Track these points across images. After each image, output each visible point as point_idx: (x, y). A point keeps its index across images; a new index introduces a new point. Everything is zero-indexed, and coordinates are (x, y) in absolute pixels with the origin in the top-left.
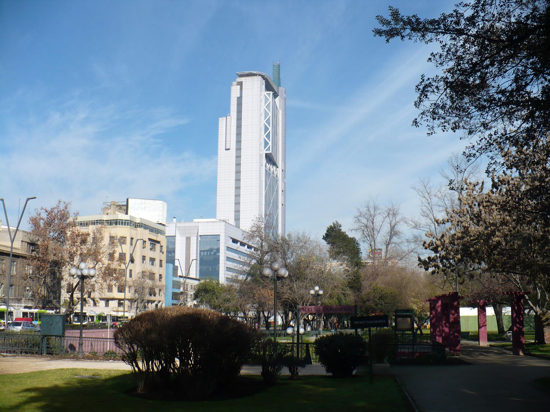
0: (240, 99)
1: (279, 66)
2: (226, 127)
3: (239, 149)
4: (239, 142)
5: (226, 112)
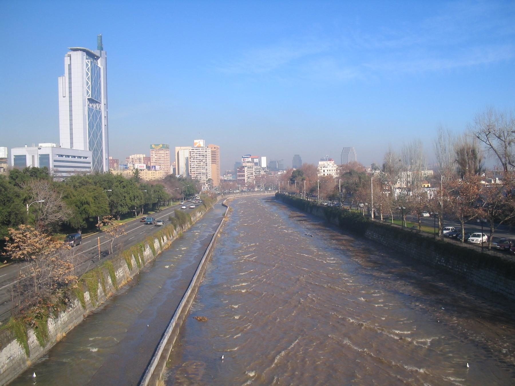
0: (70, 65)
1: (101, 37)
2: (62, 83)
3: (70, 97)
4: (70, 92)
5: (62, 74)
